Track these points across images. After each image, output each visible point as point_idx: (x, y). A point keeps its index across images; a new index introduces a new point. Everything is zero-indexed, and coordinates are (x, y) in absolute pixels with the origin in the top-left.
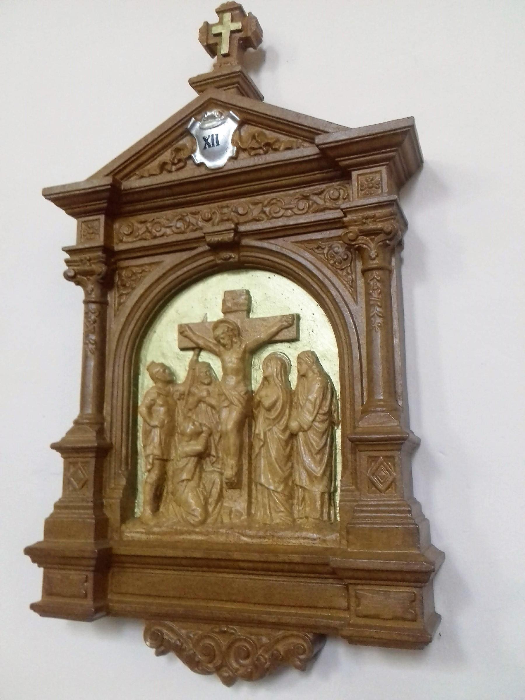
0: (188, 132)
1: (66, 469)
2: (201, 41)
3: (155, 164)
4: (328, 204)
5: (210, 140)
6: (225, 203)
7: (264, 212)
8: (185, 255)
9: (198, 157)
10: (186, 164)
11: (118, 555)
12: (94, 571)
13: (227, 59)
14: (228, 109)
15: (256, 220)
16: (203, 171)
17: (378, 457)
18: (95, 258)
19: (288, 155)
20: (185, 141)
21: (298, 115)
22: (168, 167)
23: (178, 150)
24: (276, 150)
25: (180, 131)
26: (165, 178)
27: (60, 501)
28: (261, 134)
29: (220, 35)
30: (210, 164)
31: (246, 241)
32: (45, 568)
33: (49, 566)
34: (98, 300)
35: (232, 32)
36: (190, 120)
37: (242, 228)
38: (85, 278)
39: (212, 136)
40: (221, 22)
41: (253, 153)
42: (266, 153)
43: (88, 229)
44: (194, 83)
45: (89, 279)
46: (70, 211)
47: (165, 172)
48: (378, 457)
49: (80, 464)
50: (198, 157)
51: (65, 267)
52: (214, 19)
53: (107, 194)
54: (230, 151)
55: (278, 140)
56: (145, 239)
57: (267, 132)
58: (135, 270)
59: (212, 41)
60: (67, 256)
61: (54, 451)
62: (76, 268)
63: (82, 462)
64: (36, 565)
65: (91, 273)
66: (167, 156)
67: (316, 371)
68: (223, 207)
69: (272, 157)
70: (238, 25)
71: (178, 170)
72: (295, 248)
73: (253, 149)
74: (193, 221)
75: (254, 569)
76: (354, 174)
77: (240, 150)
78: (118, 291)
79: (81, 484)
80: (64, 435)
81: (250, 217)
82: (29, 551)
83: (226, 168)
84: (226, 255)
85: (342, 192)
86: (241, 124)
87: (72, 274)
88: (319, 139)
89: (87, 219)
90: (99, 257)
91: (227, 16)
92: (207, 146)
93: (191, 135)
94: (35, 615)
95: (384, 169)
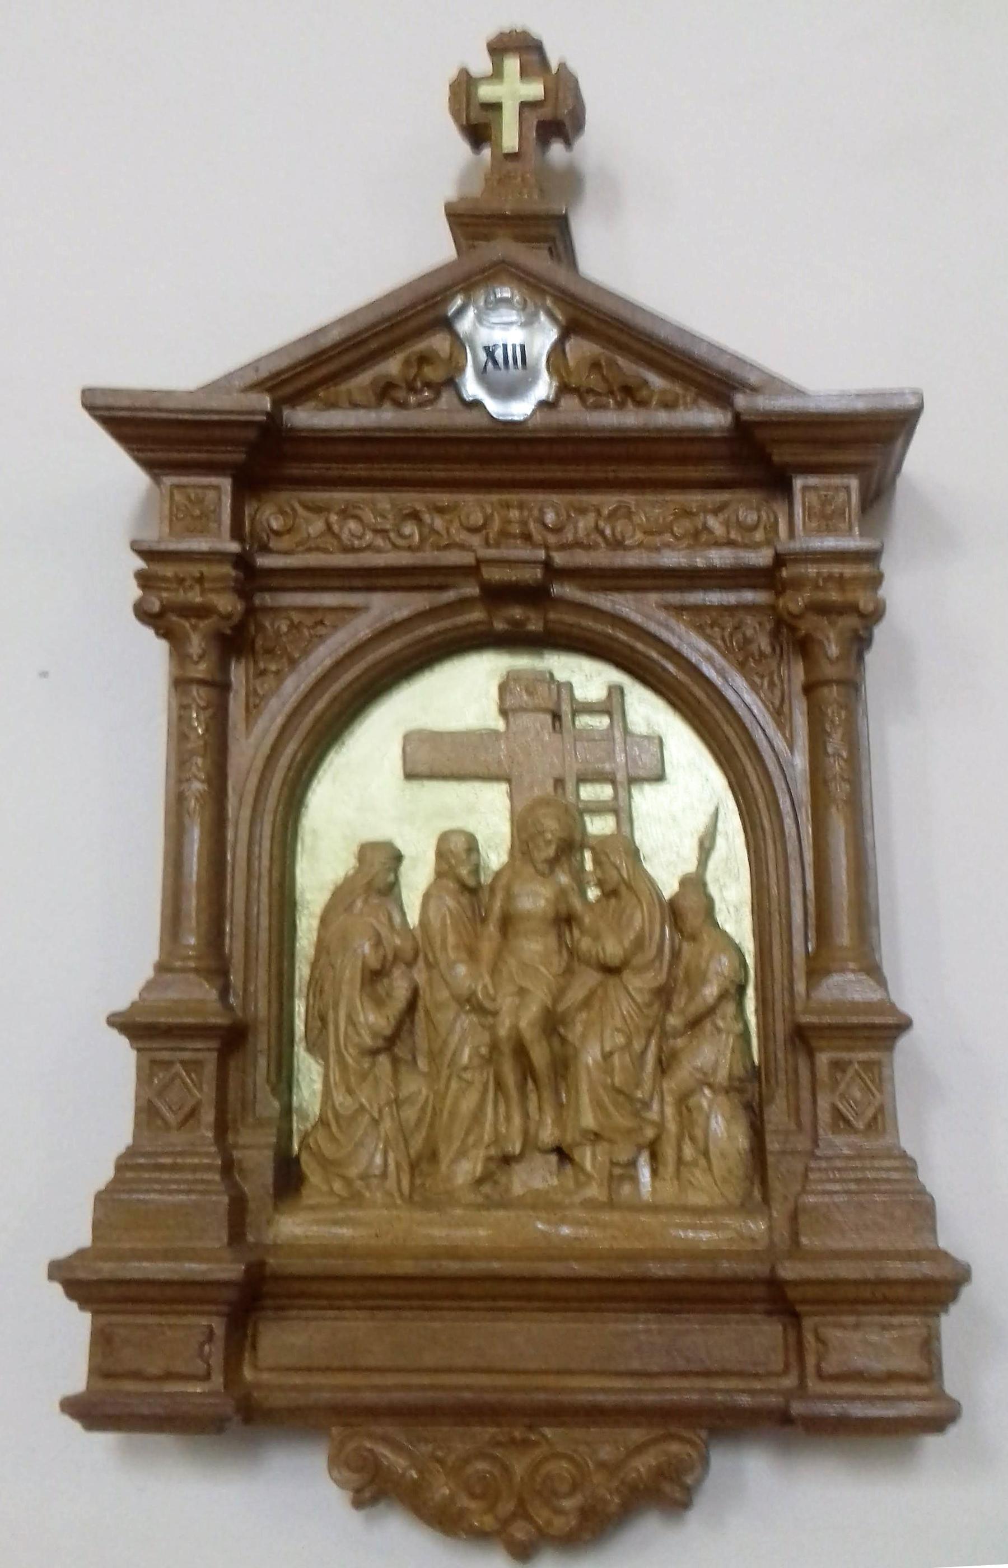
0: (447, 324)
1: (144, 1077)
2: (455, 114)
3: (365, 378)
4: (733, 535)
5: (499, 354)
6: (513, 497)
7: (602, 533)
8: (419, 601)
9: (472, 388)
10: (438, 395)
11: (279, 1278)
12: (228, 1315)
13: (510, 166)
14: (543, 293)
15: (578, 544)
16: (465, 419)
17: (850, 1062)
18: (215, 579)
19: (662, 418)
20: (439, 343)
21: (681, 331)
22: (400, 394)
23: (424, 359)
24: (642, 404)
25: (431, 315)
26: (387, 417)
27: (131, 1152)
28: (612, 364)
29: (495, 107)
30: (495, 408)
31: (556, 590)
32: (95, 1313)
33: (104, 1307)
34: (209, 677)
35: (525, 106)
36: (453, 296)
37: (559, 559)
38: (187, 625)
39: (505, 347)
40: (497, 74)
41: (591, 400)
42: (621, 406)
43: (189, 505)
44: (460, 216)
45: (194, 628)
46: (141, 455)
47: (387, 405)
48: (850, 1062)
49: (178, 1068)
50: (472, 388)
51: (135, 592)
52: (481, 64)
53: (252, 434)
54: (543, 388)
55: (646, 383)
56: (326, 551)
57: (621, 361)
58: (296, 617)
59: (477, 116)
60: (139, 564)
61: (114, 1033)
62: (165, 595)
63: (183, 1063)
64: (74, 1305)
65: (202, 612)
66: (392, 366)
67: (318, 971)
68: (508, 506)
69: (631, 418)
70: (535, 90)
71: (420, 405)
72: (662, 615)
73: (590, 391)
74: (439, 523)
75: (602, 1298)
76: (798, 483)
77: (564, 389)
78: (256, 663)
79: (181, 1116)
80: (134, 996)
81: (569, 536)
82: (59, 1271)
83: (530, 424)
84: (517, 612)
85: (764, 514)
86: (565, 334)
87: (156, 607)
88: (741, 401)
89: (184, 480)
90: (223, 578)
91: (512, 65)
92: (490, 365)
93: (455, 335)
94: (75, 1427)
95: (854, 483)
